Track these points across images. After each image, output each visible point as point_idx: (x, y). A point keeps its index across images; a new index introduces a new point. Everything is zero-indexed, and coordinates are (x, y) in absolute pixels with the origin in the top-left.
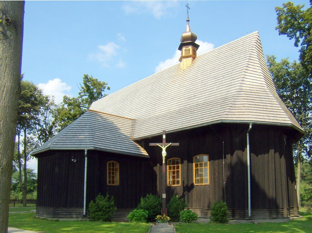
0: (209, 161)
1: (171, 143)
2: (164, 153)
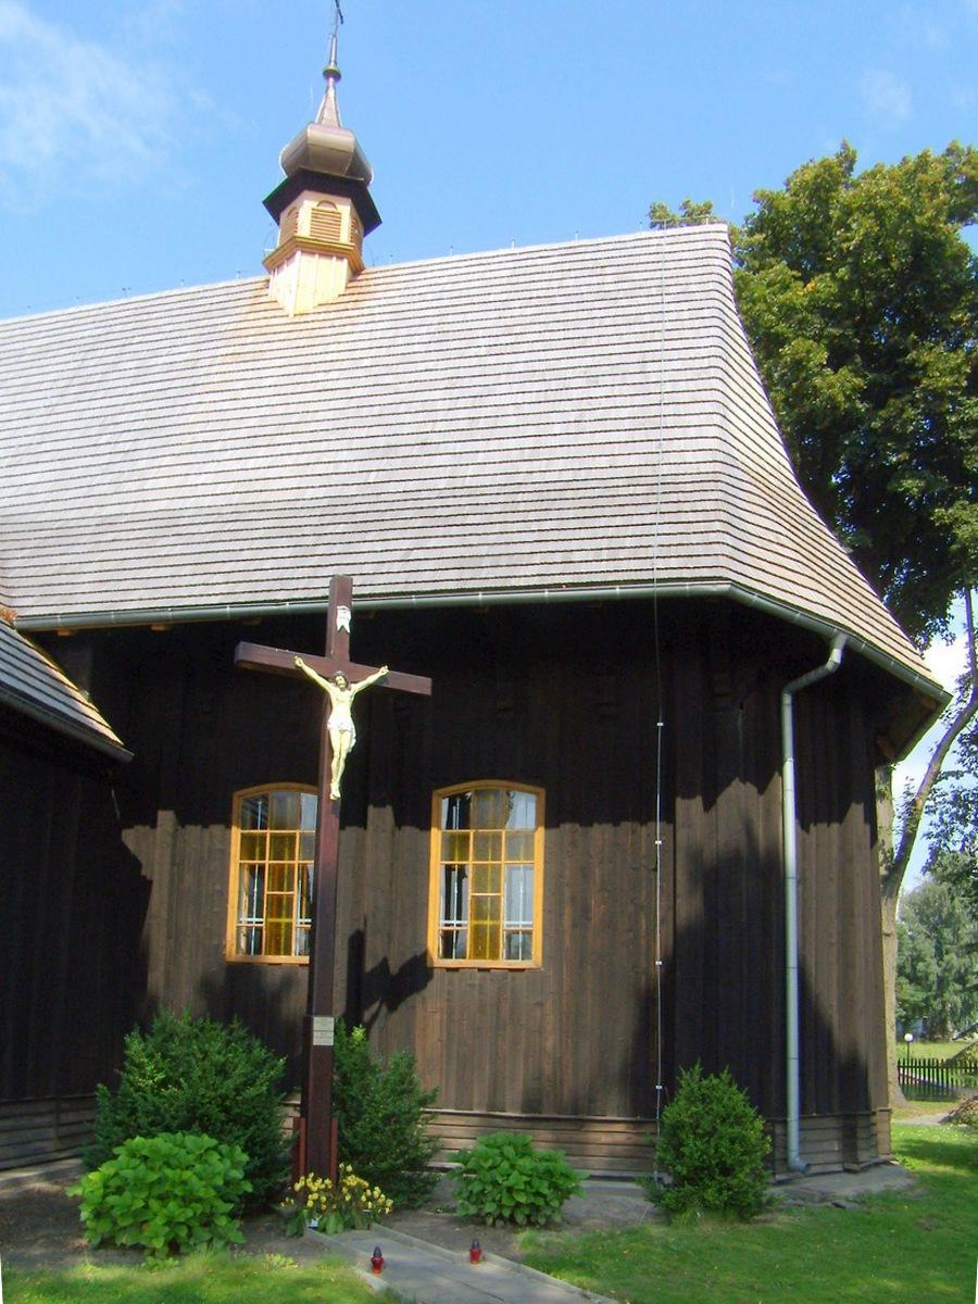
0: (547, 826)
1: (384, 670)
2: (341, 731)
